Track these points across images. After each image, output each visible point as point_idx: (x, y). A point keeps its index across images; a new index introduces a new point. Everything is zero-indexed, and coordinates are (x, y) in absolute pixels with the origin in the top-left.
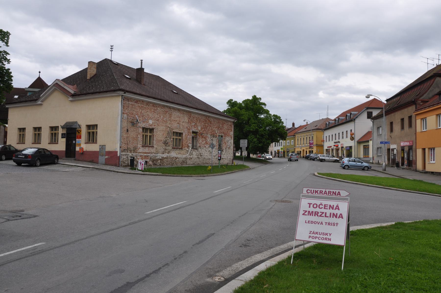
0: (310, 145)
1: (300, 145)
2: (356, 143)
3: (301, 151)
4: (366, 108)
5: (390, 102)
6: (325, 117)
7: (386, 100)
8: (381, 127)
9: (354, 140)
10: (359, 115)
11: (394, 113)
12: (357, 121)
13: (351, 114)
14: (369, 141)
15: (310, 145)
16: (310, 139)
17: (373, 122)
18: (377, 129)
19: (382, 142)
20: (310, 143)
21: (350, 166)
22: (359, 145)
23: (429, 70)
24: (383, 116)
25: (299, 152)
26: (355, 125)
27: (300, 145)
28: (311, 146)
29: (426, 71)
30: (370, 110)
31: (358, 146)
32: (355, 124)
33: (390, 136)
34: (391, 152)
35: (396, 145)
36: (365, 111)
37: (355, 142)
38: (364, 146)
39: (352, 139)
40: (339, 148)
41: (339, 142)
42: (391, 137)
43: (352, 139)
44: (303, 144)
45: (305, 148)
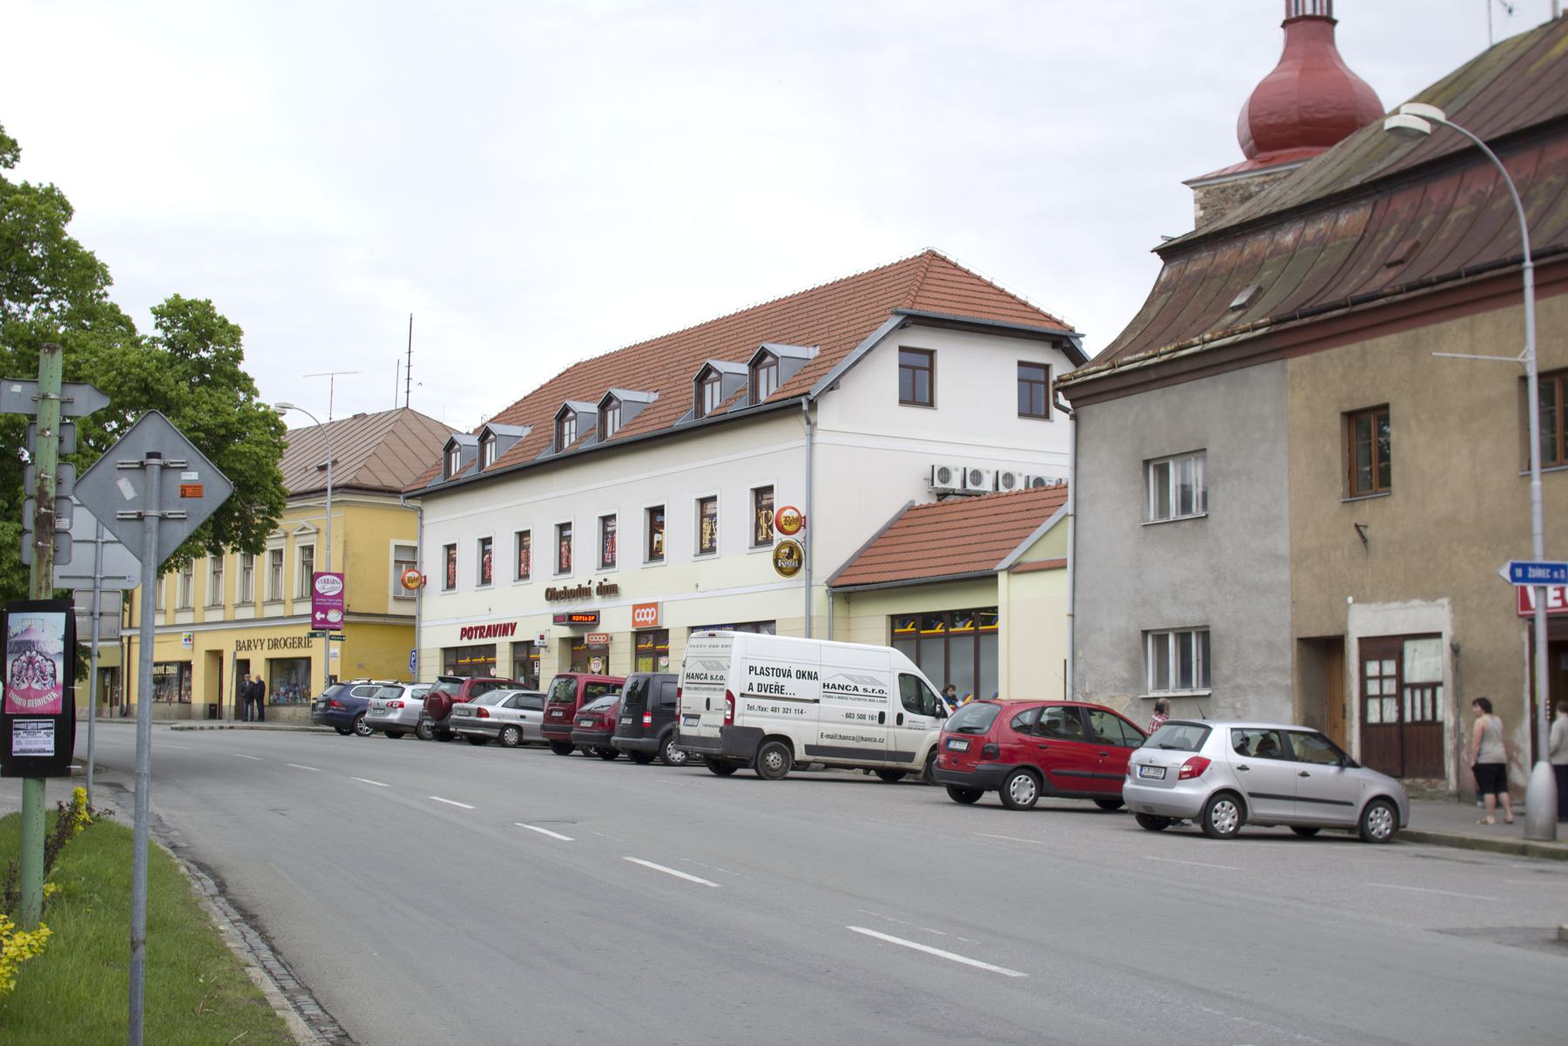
0: (319, 616)
1: (186, 618)
2: (821, 594)
3: (185, 666)
4: (897, 314)
5: (1200, 262)
6: (379, 398)
7: (1159, 242)
8: (1200, 452)
9: (802, 572)
10: (843, 374)
11: (1315, 355)
12: (828, 414)
13: (607, 403)
14: (994, 577)
15: (319, 616)
16: (308, 565)
17: (1074, 418)
18: (1141, 474)
19: (1525, 567)
20: (322, 595)
21: (1252, 795)
22: (840, 611)
23: (1496, 41)
24: (1521, 290)
25: (172, 670)
26: (818, 449)
27: (186, 618)
28: (324, 621)
29: (1476, 46)
30: (919, 339)
31: (832, 618)
32: (819, 437)
33: (1357, 526)
34: (1362, 670)
35: (1445, 601)
36: (886, 341)
37: (809, 587)
38: (893, 618)
39: (791, 563)
40: (610, 638)
41: (608, 590)
42: (1364, 540)
43: (791, 563)
44: (207, 609)
45: (226, 643)
